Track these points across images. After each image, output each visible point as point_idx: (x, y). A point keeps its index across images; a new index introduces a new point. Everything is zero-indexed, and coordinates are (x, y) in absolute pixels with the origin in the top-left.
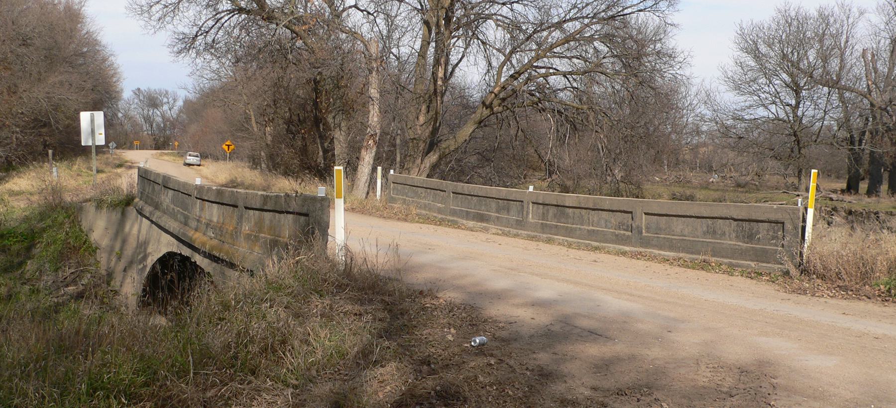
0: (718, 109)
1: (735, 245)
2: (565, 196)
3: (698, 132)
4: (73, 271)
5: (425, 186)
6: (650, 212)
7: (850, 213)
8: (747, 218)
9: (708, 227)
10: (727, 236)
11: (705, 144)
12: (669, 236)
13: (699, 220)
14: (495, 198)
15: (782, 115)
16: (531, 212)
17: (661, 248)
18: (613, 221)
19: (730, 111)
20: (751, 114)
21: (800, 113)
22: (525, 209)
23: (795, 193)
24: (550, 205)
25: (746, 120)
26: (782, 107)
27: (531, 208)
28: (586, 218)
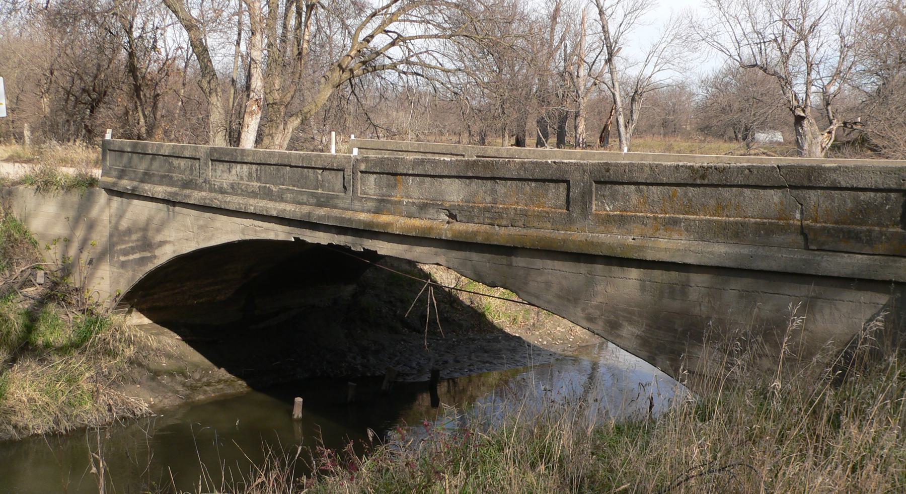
4: (23, 269)
5: (422, 150)
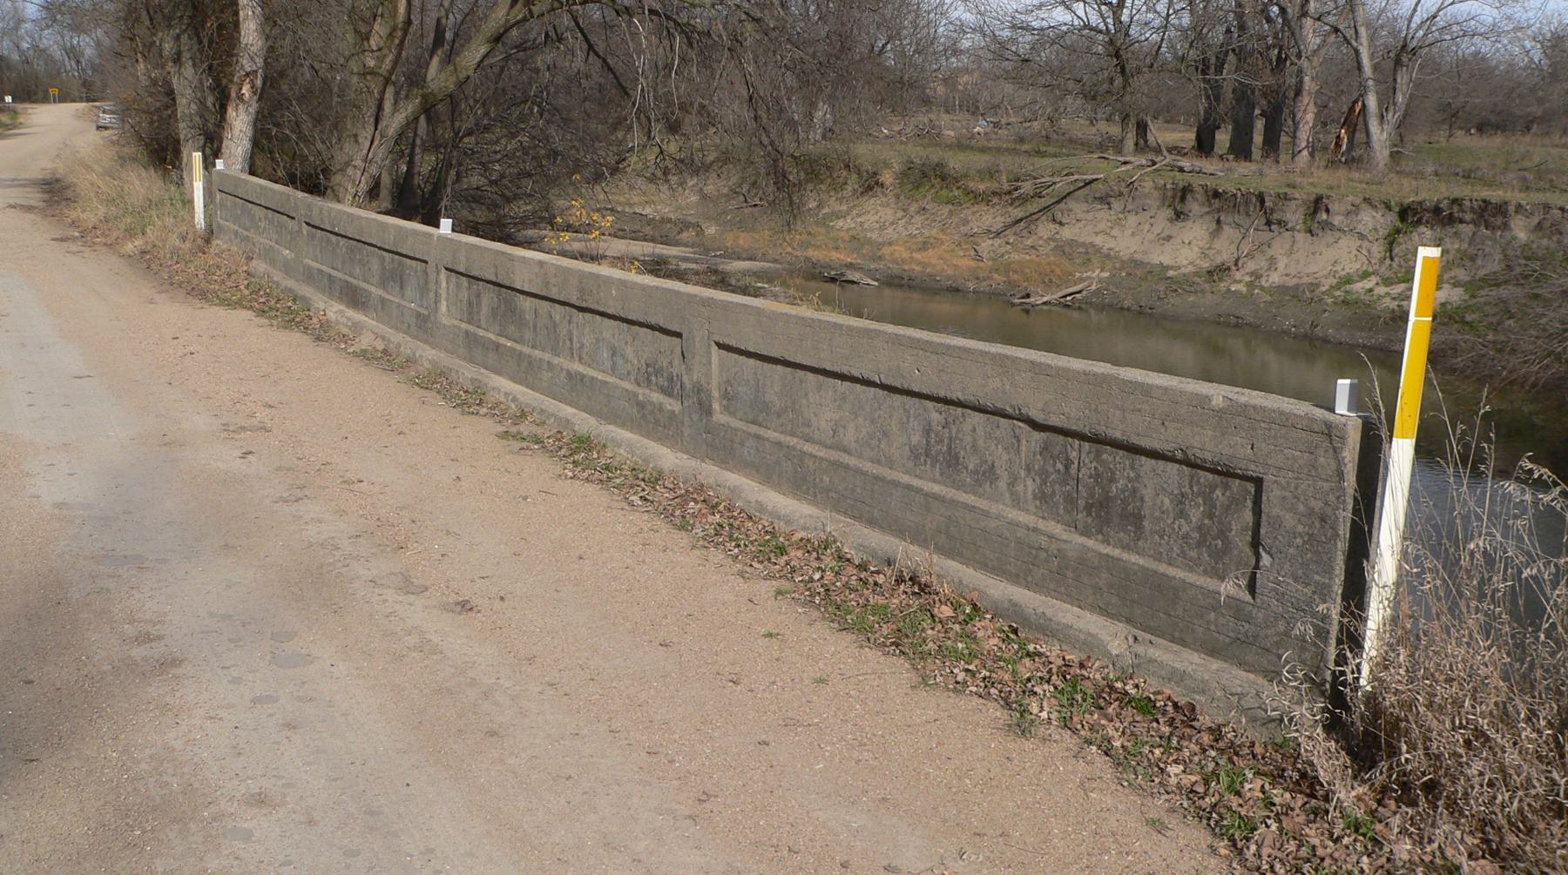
0: (986, 10)
1: (1035, 530)
2: (511, 258)
3: (957, 52)
6: (733, 343)
7: (1216, 195)
8: (1086, 430)
9: (927, 432)
10: (1002, 484)
11: (966, 70)
12: (793, 441)
13: (898, 399)
14: (375, 246)
15: (1095, 19)
16: (444, 295)
17: (767, 474)
18: (629, 351)
19: (1006, 14)
20: (1043, 19)
21: (1125, 18)
22: (432, 286)
23: (1120, 159)
24: (482, 280)
25: (1034, 29)
26: (1096, 6)
27: (444, 285)
28: (563, 330)
